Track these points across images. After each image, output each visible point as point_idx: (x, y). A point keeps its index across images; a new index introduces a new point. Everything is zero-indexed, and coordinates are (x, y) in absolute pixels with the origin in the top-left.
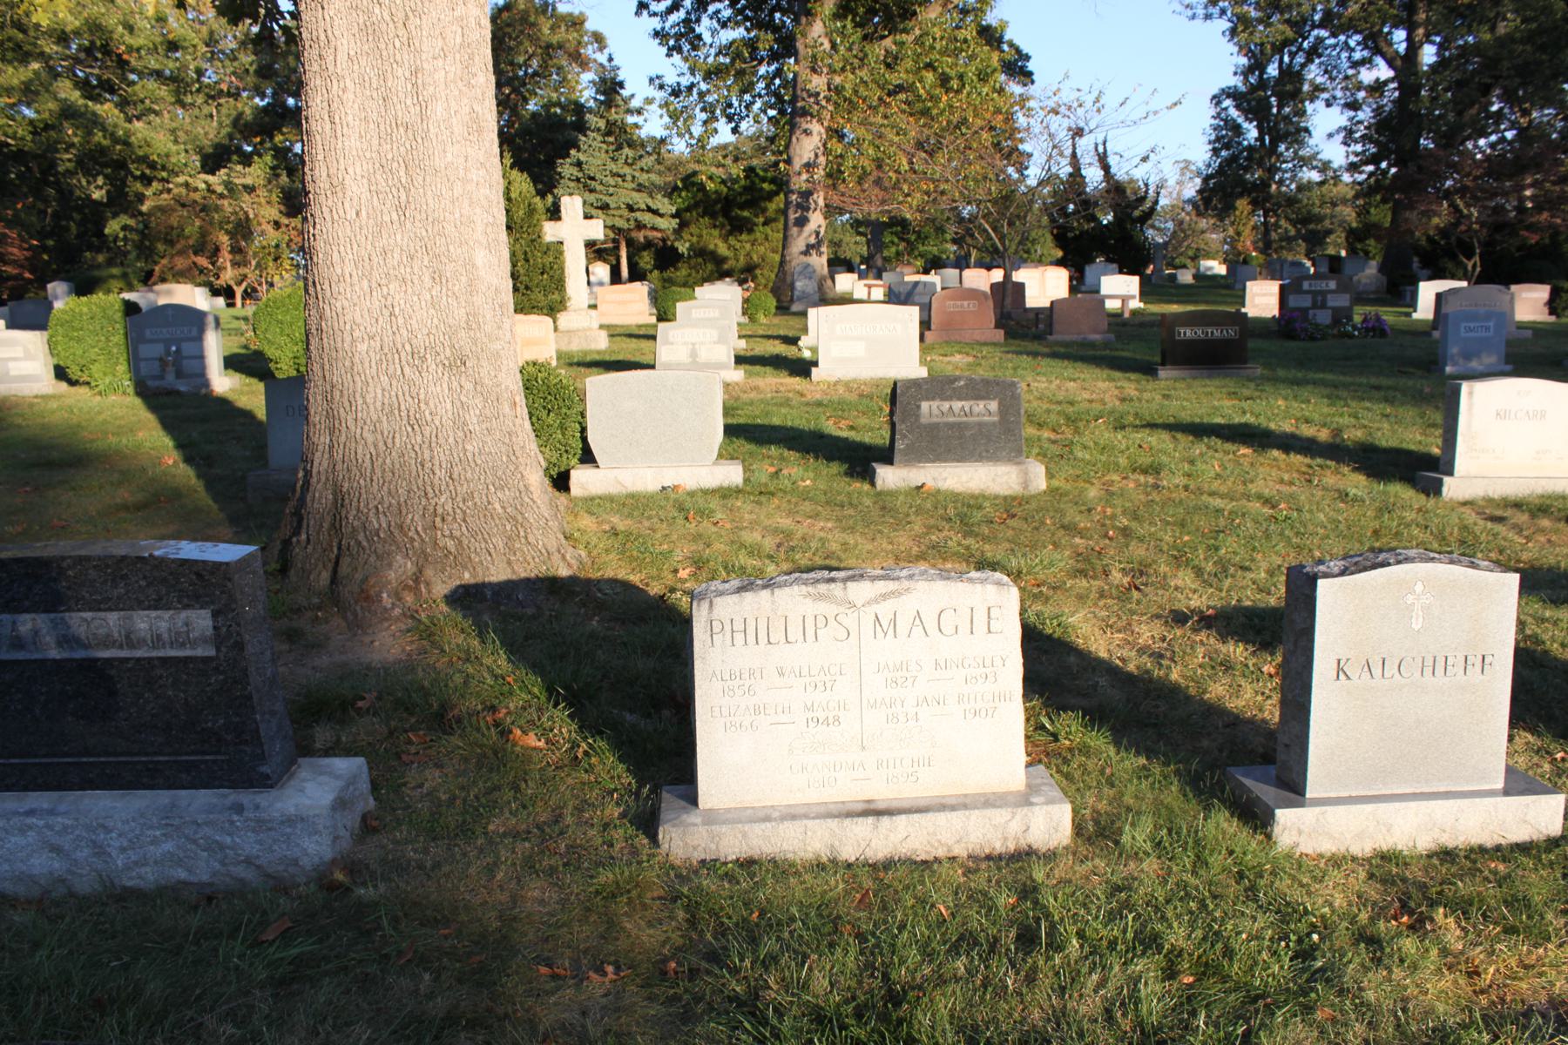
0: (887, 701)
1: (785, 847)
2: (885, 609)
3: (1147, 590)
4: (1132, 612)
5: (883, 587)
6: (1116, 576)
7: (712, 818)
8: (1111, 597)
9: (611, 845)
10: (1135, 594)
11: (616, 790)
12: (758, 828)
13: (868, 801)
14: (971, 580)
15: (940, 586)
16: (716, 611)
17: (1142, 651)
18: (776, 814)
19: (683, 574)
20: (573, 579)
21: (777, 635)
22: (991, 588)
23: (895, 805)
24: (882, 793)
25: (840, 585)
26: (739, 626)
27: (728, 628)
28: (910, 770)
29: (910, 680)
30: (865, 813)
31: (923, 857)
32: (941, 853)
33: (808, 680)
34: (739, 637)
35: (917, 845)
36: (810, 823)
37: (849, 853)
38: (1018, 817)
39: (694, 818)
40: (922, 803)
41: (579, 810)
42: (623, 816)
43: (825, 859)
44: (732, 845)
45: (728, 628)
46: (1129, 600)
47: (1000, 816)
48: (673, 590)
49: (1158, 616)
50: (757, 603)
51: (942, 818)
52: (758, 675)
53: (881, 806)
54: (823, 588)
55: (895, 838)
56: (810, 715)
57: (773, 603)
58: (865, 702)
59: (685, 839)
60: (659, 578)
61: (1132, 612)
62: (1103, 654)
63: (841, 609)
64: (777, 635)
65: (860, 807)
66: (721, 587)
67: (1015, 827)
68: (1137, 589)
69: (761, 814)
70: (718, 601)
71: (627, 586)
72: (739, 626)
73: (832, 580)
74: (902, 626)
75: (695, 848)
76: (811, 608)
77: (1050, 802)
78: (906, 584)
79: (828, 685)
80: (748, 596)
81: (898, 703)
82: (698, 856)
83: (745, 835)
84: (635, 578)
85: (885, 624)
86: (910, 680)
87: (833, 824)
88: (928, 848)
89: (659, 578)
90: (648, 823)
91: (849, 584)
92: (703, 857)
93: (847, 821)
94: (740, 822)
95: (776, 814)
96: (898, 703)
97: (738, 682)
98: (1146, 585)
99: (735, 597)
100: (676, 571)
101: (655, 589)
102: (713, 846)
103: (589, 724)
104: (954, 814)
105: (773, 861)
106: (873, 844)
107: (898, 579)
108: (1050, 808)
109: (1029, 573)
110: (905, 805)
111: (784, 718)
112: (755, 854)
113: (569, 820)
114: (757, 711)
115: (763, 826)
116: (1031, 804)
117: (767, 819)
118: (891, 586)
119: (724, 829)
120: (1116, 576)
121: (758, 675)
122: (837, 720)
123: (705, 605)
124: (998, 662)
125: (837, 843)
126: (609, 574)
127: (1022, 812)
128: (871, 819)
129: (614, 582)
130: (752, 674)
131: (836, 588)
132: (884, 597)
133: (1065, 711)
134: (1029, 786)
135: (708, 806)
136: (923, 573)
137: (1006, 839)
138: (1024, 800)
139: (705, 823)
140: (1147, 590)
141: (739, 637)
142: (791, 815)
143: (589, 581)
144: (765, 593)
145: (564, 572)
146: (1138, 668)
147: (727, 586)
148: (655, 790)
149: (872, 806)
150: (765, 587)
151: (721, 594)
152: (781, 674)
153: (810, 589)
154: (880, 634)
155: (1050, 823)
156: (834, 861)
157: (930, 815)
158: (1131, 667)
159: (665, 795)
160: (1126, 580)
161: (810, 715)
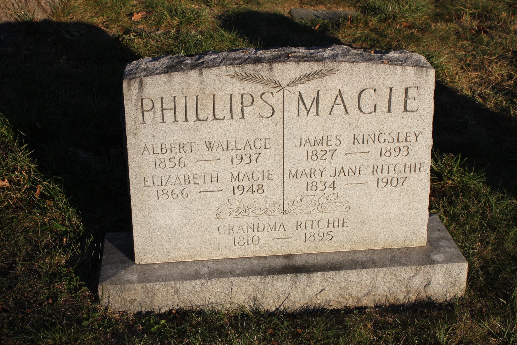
0: (308, 171)
1: (213, 299)
2: (308, 89)
3: (494, 33)
4: (484, 53)
5: (307, 67)
6: (466, 20)
7: (150, 274)
8: (466, 39)
9: (55, 299)
10: (485, 38)
11: (66, 233)
12: (189, 285)
13: (288, 257)
14: (391, 62)
15: (361, 67)
16: (145, 90)
17: (498, 88)
18: (205, 271)
19: (137, 17)
20: (46, 22)
21: (206, 113)
22: (410, 70)
23: (312, 260)
24: (298, 246)
25: (266, 66)
26: (168, 104)
27: (158, 105)
28: (326, 230)
29: (329, 154)
30: (285, 270)
31: (335, 306)
32: (351, 303)
33: (234, 153)
34: (169, 115)
35: (330, 297)
36: (235, 280)
37: (269, 304)
38: (421, 274)
39: (131, 275)
40: (336, 259)
41: (30, 257)
42: (70, 263)
43: (248, 309)
44: (165, 297)
45: (158, 105)
46: (481, 42)
47: (404, 273)
48: (127, 32)
49: (506, 58)
50: (185, 83)
51: (353, 275)
52: (187, 148)
53: (299, 262)
54: (249, 68)
55: (311, 292)
56: (237, 184)
57: (201, 82)
58: (287, 172)
59: (122, 296)
60: (117, 20)
61: (484, 53)
62: (467, 92)
63: (267, 89)
64: (206, 113)
65: (280, 263)
66: (151, 66)
67: (418, 282)
68: (486, 32)
69: (191, 270)
70: (148, 80)
71: (92, 28)
72: (168, 104)
73: (258, 61)
74: (325, 104)
75: (132, 302)
76: (237, 87)
77: (449, 260)
78: (330, 65)
79: (254, 158)
80: (178, 77)
81: (318, 173)
82: (135, 308)
83: (176, 291)
84: (98, 21)
85: (308, 103)
86: (329, 154)
87: (256, 280)
88: (340, 299)
89: (117, 20)
90: (91, 273)
91: (275, 65)
92: (139, 309)
93: (269, 278)
94: (173, 279)
95: (205, 271)
96: (318, 173)
97: (168, 155)
98: (491, 28)
99: (164, 78)
100: (131, 15)
101: (114, 30)
102: (148, 301)
103: (46, 168)
104: (364, 271)
105: (200, 313)
106: (291, 297)
107: (322, 60)
108: (449, 266)
109: (402, 17)
110: (320, 261)
111: (212, 187)
112: (187, 306)
113: (20, 269)
114: (187, 180)
115: (193, 283)
116: (433, 262)
117: (196, 276)
118: (316, 67)
119: (158, 285)
120: (466, 20)
121: (187, 148)
122: (261, 187)
123: (135, 84)
124: (412, 138)
125: (259, 296)
126: (77, 17)
127: (425, 269)
128: (289, 277)
129: (79, 25)
130: (181, 147)
131: (263, 69)
132: (309, 77)
133: (447, 152)
134: (430, 241)
135: (144, 262)
136: (346, 54)
137: (408, 292)
138: (425, 257)
139: (141, 281)
140: (494, 33)
141: (169, 115)
142: (220, 270)
143: (60, 24)
144: (193, 74)
145: (39, 16)
146: (496, 104)
147: (157, 64)
148: (100, 239)
149: (291, 262)
150: (193, 67)
151: (151, 73)
152: (210, 148)
153: (237, 69)
154: (303, 112)
155: (449, 279)
156: (256, 312)
157: (343, 272)
158: (490, 105)
159: (108, 245)
160: (475, 24)
161: (237, 184)
